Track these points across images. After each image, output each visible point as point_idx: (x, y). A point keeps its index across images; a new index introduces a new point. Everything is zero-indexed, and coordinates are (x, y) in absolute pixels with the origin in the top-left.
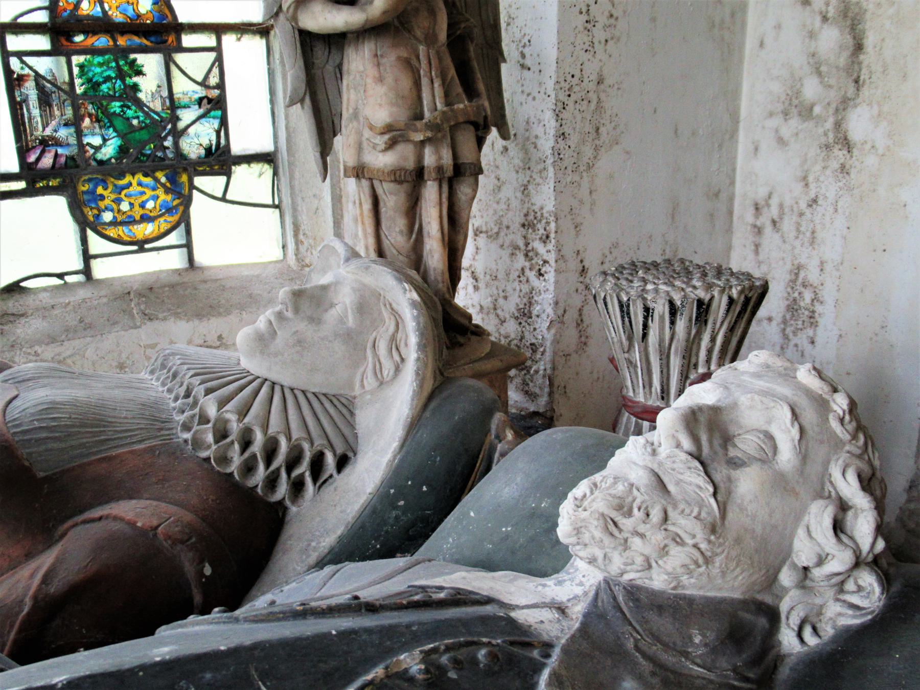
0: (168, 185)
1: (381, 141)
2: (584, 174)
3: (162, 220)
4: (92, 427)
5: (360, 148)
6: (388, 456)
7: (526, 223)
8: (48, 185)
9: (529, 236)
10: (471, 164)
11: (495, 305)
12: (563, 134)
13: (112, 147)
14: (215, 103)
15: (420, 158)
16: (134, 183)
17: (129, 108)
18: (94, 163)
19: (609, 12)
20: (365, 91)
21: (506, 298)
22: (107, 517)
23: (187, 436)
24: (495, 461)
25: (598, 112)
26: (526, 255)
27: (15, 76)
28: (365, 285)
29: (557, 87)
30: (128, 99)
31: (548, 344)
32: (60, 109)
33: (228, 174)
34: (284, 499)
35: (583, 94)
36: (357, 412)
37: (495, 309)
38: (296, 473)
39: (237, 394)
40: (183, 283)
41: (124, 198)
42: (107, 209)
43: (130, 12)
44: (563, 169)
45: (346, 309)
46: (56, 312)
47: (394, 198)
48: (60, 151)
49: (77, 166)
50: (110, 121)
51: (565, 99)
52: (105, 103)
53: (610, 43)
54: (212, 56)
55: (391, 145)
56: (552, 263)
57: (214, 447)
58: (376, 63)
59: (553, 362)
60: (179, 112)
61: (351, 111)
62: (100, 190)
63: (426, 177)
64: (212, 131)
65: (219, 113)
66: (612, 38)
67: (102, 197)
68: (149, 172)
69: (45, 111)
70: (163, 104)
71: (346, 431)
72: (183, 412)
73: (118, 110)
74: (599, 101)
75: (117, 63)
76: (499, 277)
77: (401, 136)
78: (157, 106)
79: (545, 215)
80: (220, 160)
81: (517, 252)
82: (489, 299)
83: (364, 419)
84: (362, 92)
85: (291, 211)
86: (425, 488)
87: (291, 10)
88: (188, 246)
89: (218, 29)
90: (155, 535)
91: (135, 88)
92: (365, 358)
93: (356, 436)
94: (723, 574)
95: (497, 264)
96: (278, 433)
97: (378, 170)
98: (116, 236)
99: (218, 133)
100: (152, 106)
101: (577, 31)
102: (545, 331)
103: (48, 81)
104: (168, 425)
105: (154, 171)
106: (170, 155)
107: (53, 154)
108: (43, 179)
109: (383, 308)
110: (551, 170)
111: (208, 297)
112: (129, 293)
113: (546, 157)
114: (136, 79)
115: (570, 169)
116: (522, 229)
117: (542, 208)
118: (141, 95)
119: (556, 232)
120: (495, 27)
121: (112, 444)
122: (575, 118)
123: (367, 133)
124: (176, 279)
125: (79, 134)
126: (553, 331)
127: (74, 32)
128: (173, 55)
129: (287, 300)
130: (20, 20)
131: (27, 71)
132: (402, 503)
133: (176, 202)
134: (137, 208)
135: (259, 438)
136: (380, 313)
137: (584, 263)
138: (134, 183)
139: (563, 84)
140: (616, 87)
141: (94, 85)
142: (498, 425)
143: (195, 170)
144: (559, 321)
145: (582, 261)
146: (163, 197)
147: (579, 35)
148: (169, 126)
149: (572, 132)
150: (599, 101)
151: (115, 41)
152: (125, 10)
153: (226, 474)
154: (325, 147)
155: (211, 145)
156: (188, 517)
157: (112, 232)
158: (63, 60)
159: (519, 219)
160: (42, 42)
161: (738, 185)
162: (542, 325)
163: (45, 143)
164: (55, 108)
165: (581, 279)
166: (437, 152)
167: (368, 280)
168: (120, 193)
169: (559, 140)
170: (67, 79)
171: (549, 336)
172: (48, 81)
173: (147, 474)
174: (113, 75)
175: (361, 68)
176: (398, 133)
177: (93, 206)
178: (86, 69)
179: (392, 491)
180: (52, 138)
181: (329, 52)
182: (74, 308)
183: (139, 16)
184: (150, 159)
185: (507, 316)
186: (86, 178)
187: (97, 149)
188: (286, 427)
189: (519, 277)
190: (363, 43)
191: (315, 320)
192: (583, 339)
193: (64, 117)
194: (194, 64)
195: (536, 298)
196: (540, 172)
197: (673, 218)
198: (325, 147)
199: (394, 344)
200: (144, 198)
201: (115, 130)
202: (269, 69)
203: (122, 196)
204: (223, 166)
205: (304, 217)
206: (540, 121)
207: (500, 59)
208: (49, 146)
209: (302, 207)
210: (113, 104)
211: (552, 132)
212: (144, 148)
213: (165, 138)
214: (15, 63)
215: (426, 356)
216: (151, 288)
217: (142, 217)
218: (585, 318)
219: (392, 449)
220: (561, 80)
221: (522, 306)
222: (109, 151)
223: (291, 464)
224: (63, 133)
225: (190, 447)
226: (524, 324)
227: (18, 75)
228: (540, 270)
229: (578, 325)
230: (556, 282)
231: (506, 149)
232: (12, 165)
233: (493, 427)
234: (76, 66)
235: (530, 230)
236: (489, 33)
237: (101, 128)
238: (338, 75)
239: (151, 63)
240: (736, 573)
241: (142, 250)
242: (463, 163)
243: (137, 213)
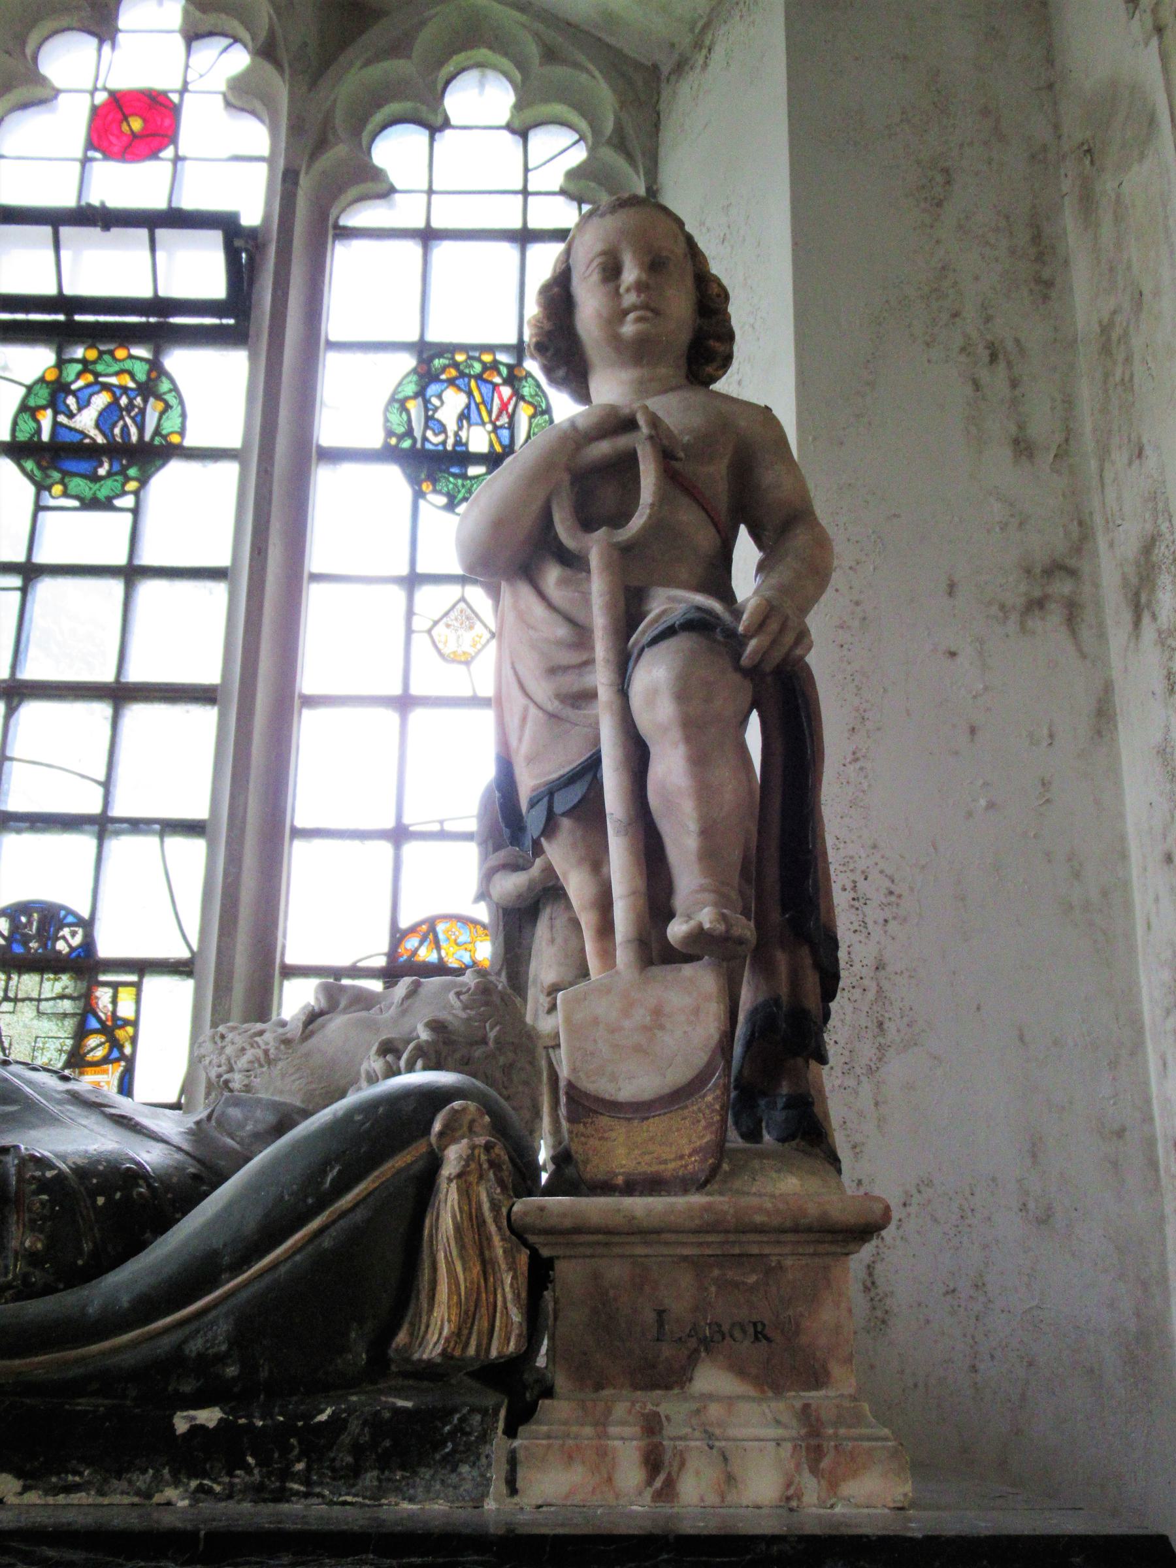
2: (864, 1079)
53: (893, 926)
74: (880, 990)
94: (283, 1076)
130: (360, 964)
150: (880, 990)
161: (1158, 1122)
192: (879, 1313)
197: (1034, 1156)
229: (867, 1289)
240: (293, 1078)
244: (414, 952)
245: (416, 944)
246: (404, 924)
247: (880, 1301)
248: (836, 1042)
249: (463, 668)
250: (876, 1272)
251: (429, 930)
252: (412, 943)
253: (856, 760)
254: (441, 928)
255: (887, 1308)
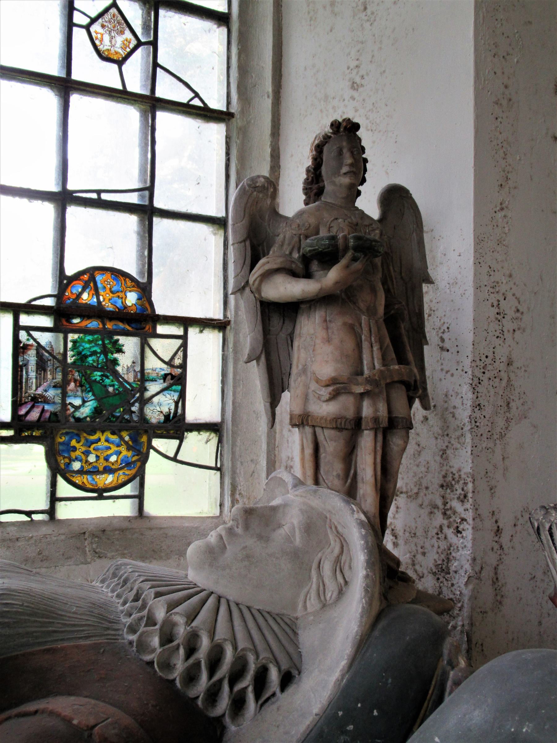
0: (130, 443)
1: (325, 392)
2: (498, 442)
3: (121, 472)
4: (42, 617)
5: (306, 399)
6: (337, 674)
7: (445, 484)
8: (32, 434)
9: (447, 496)
10: (403, 418)
11: (413, 561)
12: (479, 405)
13: (89, 408)
14: (177, 380)
15: (359, 409)
16: (103, 439)
17: (107, 377)
18: (72, 420)
19: (516, 307)
20: (313, 351)
21: (424, 554)
22: (43, 711)
23: (133, 637)
24: (448, 690)
25: (509, 389)
26: (444, 514)
27: (22, 345)
28: (312, 508)
29: (474, 364)
30: (108, 370)
31: (466, 599)
32: (52, 374)
33: (181, 439)
34: (223, 715)
35: (495, 372)
36: (300, 632)
37: (413, 565)
38: (239, 686)
39: (185, 601)
40: (132, 528)
41: (93, 451)
42: (77, 459)
43: (119, 304)
44: (479, 435)
45: (294, 528)
46: (19, 544)
47: (334, 444)
48: (47, 407)
49: (58, 421)
50: (91, 387)
51: (480, 375)
52: (88, 372)
53: (518, 333)
54: (179, 342)
55: (334, 396)
56: (470, 520)
57: (159, 650)
58: (325, 327)
59: (471, 618)
60: (147, 384)
61: (300, 367)
62: (73, 443)
63: (363, 427)
64: (172, 401)
65: (179, 388)
66: (519, 329)
67: (74, 449)
68: (116, 431)
69: (40, 374)
70: (135, 377)
71: (291, 650)
72: (130, 615)
73: (98, 378)
75: (103, 342)
76: (417, 534)
77: (344, 388)
78: (130, 378)
79: (463, 476)
80: (176, 426)
81: (436, 511)
82: (408, 555)
83: (308, 638)
84: (311, 351)
85: (230, 473)
86: (375, 713)
87: (257, 283)
88: (140, 497)
89: (186, 322)
90: (90, 736)
91: (115, 362)
92: (310, 578)
93: (300, 654)
95: (416, 522)
96: (225, 640)
97: (322, 418)
98: (80, 483)
99: (177, 403)
100: (126, 377)
101: (489, 320)
102: (463, 586)
103: (47, 351)
104: (116, 626)
105: (120, 431)
106: (135, 418)
107: (40, 409)
108: (28, 429)
109: (329, 531)
110: (468, 438)
111: (152, 542)
112: (84, 533)
113: (464, 425)
114: (116, 355)
115: (485, 436)
116: (441, 489)
117: (460, 470)
118: (119, 369)
119: (473, 492)
120: (420, 315)
121: (60, 636)
122: (489, 392)
123: (313, 386)
124: (126, 524)
125: (64, 395)
126: (471, 587)
127: (74, 315)
128: (148, 339)
129: (239, 518)
130: (34, 303)
131: (31, 342)
132: (351, 727)
133: (135, 458)
134: (102, 460)
135: (205, 643)
136: (326, 535)
137: (499, 524)
138: (103, 439)
139: (478, 363)
140: (523, 369)
141: (82, 357)
142: (450, 651)
143: (154, 432)
144: (476, 577)
145: (496, 522)
146: (125, 453)
147: (492, 324)
148: (138, 395)
149: (486, 404)
151: (104, 325)
152: (116, 302)
153: (168, 681)
154: (274, 401)
155: (170, 413)
156: (127, 720)
157: (77, 480)
158: (61, 336)
159: (438, 480)
160: (46, 321)
162: (460, 580)
163: (35, 400)
164: (49, 373)
165: (496, 539)
166: (374, 404)
167: (316, 503)
168: (90, 447)
169: (476, 410)
170: (62, 351)
171: (467, 592)
172: (47, 351)
173: (89, 671)
174: (99, 351)
175: (312, 331)
176: (342, 385)
177: (66, 455)
178: (78, 344)
179: (340, 713)
180: (42, 396)
181: (284, 323)
182: (36, 541)
183: (126, 307)
184: (118, 421)
185: (425, 572)
186: (64, 431)
187: (77, 408)
188: (234, 638)
189: (437, 534)
190: (315, 311)
191: (263, 538)
192: (499, 598)
193: (54, 381)
194: (165, 348)
195: (453, 554)
196: (458, 438)
198: (274, 401)
199: (339, 566)
200: (109, 452)
201: (94, 395)
202: (223, 355)
203: (91, 449)
204: (177, 431)
205: (241, 479)
206: (457, 394)
207: (423, 341)
208: (38, 402)
209: (240, 470)
210: (96, 373)
211: (469, 403)
212: (115, 411)
213: (133, 404)
214: (23, 335)
215: (375, 574)
216: (104, 531)
217: (105, 468)
218: (500, 577)
219: (341, 667)
220: (477, 359)
221: (439, 562)
222: (86, 411)
223: (236, 675)
224: (51, 393)
225: (134, 649)
226: (442, 579)
227: (24, 344)
228: (458, 527)
229: (494, 583)
230: (474, 539)
231: (426, 418)
232: (6, 416)
233: (446, 652)
234: (71, 341)
235: (448, 491)
236: (414, 320)
237: (82, 391)
238: (290, 342)
239: (130, 344)
241: (100, 497)
242: (396, 417)
243: (102, 465)
244: (79, 295)
245: (80, 290)
246: (70, 271)
247: (499, 589)
248: (484, 417)
249: (115, 67)
250: (499, 571)
251: (89, 276)
252: (77, 288)
253: (502, 209)
254: (99, 278)
255: (502, 593)
